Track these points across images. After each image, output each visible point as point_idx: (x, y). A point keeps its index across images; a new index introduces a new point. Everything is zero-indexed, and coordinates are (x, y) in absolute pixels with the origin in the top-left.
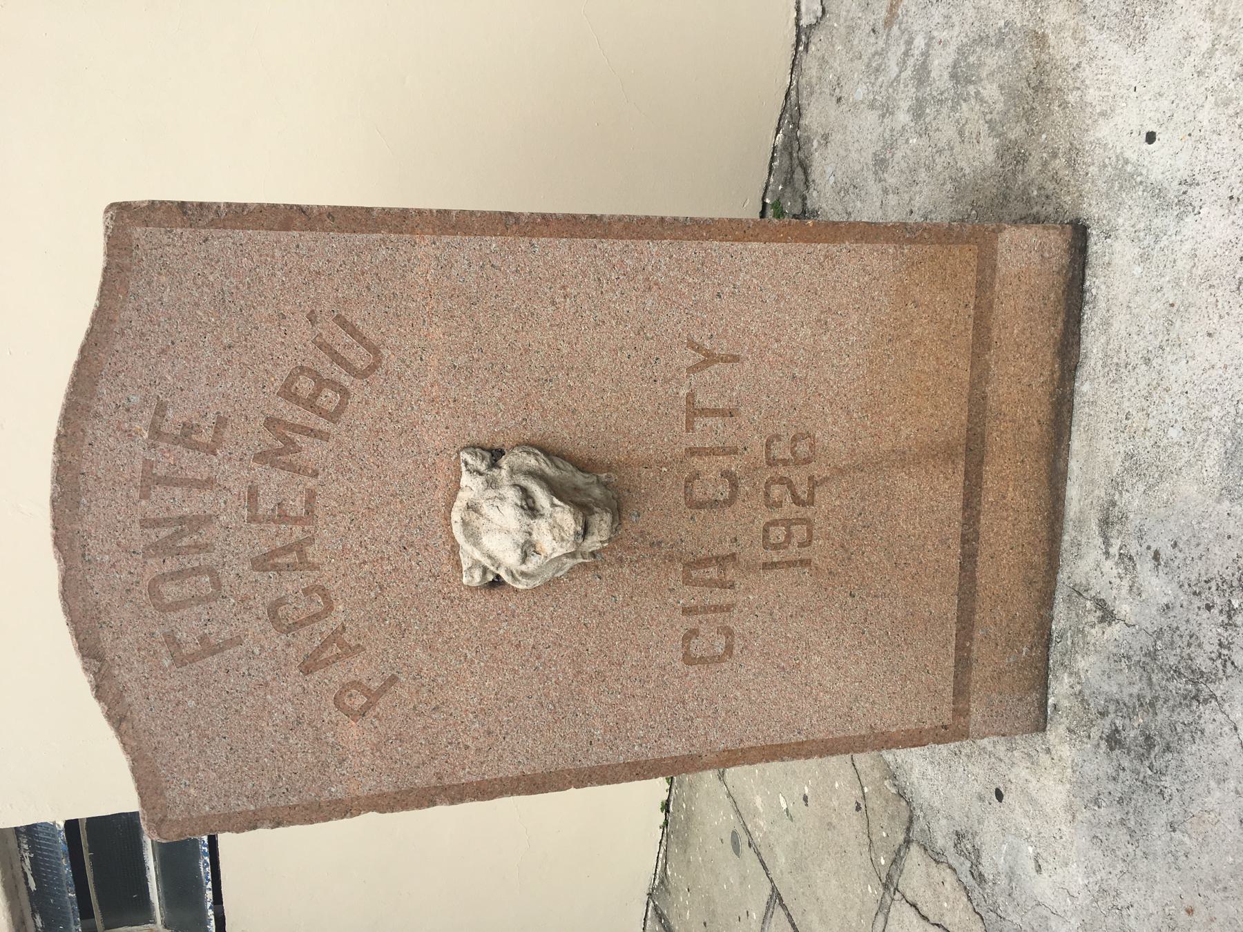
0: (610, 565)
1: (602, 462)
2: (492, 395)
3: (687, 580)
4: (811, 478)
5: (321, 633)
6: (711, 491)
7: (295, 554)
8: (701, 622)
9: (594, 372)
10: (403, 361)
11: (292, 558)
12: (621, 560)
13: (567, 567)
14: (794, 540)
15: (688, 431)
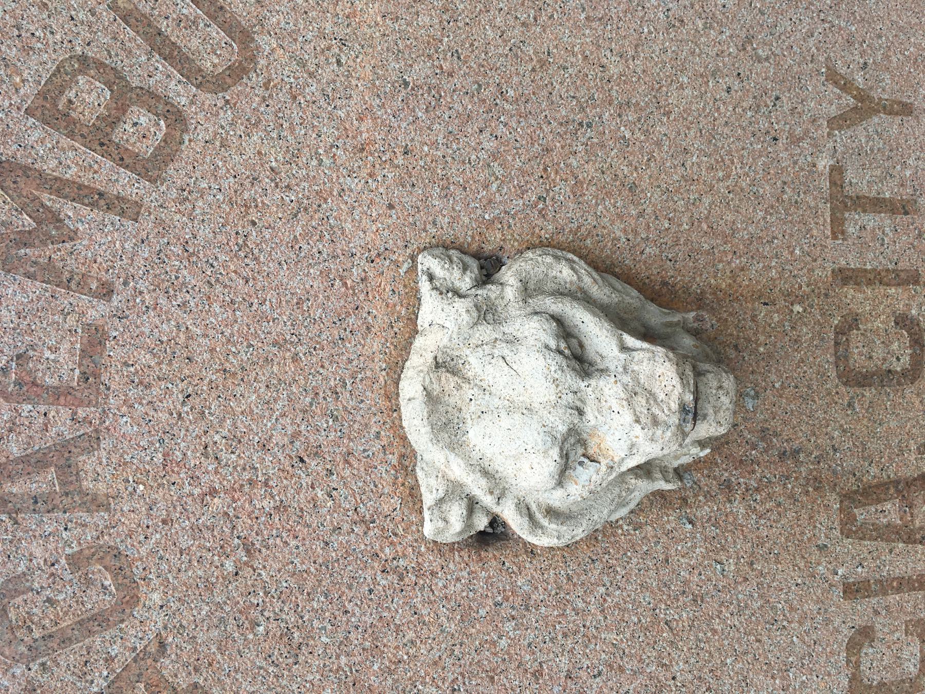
0: (709, 496)
2: (479, 147)
3: (850, 528)
5: (109, 660)
6: (879, 353)
7: (52, 471)
8: (876, 613)
10: (302, 64)
11: (45, 482)
12: (727, 486)
13: (637, 496)
15: (835, 237)
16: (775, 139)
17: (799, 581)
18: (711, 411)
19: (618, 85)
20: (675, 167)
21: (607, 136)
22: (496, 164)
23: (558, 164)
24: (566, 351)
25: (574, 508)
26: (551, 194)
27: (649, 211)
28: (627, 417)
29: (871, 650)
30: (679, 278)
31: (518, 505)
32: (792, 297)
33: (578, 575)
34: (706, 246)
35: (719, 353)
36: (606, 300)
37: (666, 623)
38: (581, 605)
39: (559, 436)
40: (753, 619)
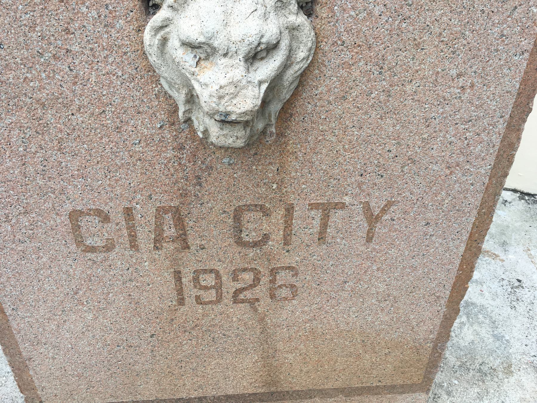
0: (176, 138)
1: (287, 127)
3: (161, 211)
4: (257, 300)
6: (251, 226)
8: (117, 224)
9: (381, 118)
12: (181, 148)
14: (202, 292)
15: (309, 205)
16: (361, 175)
17: (132, 185)
18: (225, 132)
19: (400, 90)
20: (353, 122)
21: (374, 84)
22: (365, 15)
23: (361, 54)
24: (260, 48)
25: (167, 56)
26: (345, 49)
27: (331, 107)
28: (223, 82)
29: (97, 221)
30: (294, 123)
31: (168, 19)
32: (281, 183)
33: (128, 59)
34: (310, 138)
35: (253, 145)
36: (285, 78)
37: (104, 111)
38: (110, 60)
39: (211, 41)
40: (110, 160)
